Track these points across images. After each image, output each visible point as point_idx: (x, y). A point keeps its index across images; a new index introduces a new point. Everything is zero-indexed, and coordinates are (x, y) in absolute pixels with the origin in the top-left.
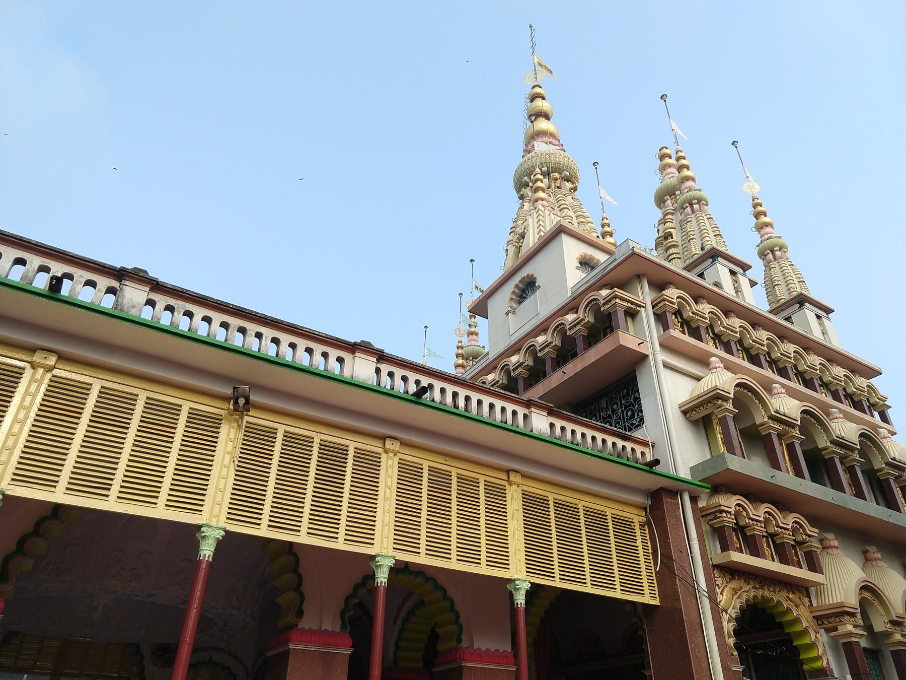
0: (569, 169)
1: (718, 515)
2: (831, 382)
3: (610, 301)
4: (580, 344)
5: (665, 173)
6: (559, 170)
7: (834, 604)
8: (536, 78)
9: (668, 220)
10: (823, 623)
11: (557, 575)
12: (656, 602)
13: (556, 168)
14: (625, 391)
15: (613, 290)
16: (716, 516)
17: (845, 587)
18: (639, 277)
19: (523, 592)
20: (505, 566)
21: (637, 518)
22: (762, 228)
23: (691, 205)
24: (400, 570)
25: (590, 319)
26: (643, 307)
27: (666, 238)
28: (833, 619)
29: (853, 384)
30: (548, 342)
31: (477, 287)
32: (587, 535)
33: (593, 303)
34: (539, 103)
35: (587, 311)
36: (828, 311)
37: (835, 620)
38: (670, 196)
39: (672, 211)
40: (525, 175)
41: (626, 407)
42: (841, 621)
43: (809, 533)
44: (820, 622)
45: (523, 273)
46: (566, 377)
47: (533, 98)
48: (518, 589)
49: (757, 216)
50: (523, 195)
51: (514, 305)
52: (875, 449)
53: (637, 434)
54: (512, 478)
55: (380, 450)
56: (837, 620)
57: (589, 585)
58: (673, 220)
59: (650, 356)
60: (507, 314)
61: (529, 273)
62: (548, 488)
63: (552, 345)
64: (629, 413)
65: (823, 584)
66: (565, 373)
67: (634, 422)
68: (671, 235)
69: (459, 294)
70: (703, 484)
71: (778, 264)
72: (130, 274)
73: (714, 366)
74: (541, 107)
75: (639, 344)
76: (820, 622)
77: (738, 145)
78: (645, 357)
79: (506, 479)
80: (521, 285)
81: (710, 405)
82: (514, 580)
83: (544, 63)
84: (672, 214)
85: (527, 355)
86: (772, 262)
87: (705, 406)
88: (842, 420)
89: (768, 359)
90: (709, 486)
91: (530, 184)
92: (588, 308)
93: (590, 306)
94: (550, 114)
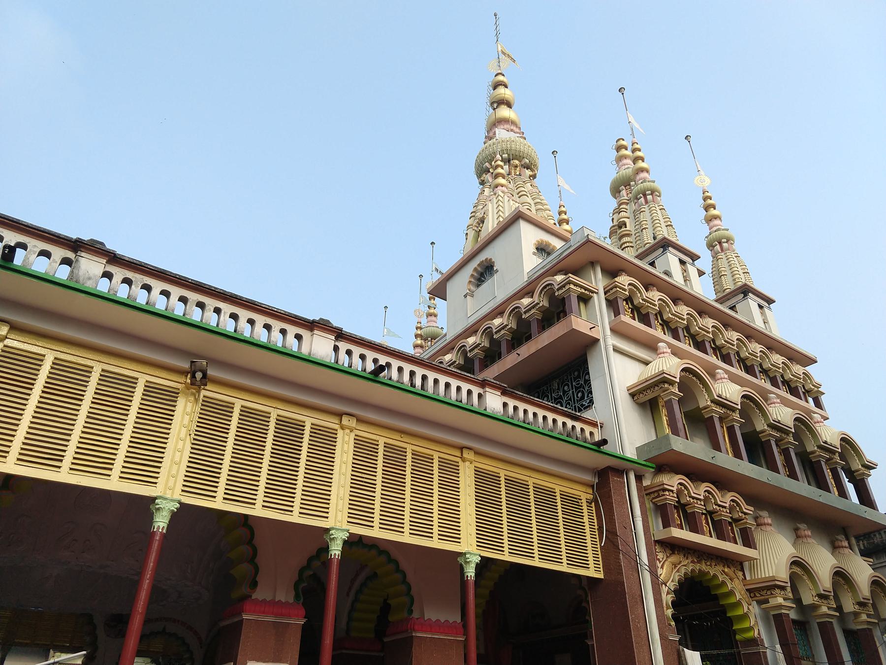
0: (529, 156)
1: (661, 493)
2: (725, 345)
3: (564, 286)
4: (534, 327)
5: (621, 164)
6: (520, 158)
7: (766, 577)
8: (499, 66)
9: (622, 210)
10: (755, 596)
11: (506, 549)
12: (601, 576)
13: (516, 155)
14: (576, 373)
15: (567, 276)
16: (659, 494)
17: (776, 562)
18: (593, 264)
19: (473, 565)
20: (457, 540)
21: (584, 495)
22: (710, 220)
23: (645, 195)
24: (354, 543)
25: (545, 303)
26: (596, 293)
27: (620, 227)
28: (765, 592)
29: (791, 371)
30: (504, 325)
31: (437, 270)
32: (507, 504)
33: (548, 288)
34: (501, 90)
35: (542, 296)
36: (770, 301)
37: (766, 593)
38: (625, 187)
39: (626, 201)
40: (486, 160)
41: (577, 388)
42: (772, 594)
43: (745, 510)
44: (752, 595)
45: (482, 257)
46: (520, 359)
47: (496, 86)
48: (469, 562)
49: (707, 208)
50: (484, 180)
51: (473, 288)
52: (808, 433)
53: (587, 415)
54: (465, 455)
55: (336, 427)
56: (769, 593)
57: (536, 559)
58: (627, 209)
59: (601, 340)
60: (465, 296)
61: (487, 257)
62: (500, 465)
63: (508, 327)
64: (580, 395)
65: (756, 559)
66: (519, 355)
67: (584, 403)
68: (625, 224)
69: (419, 276)
70: (648, 464)
71: (725, 256)
72: (86, 246)
73: (662, 351)
74: (504, 95)
75: (590, 329)
76: (752, 595)
77: (691, 140)
78: (596, 341)
79: (460, 456)
80: (479, 269)
81: (656, 388)
82: (465, 554)
83: (507, 52)
84: (627, 204)
85: (484, 337)
86: (720, 253)
87: (652, 389)
88: (779, 405)
89: (713, 346)
90: (654, 466)
91: (490, 170)
92: (543, 293)
93: (545, 290)
94: (512, 102)
